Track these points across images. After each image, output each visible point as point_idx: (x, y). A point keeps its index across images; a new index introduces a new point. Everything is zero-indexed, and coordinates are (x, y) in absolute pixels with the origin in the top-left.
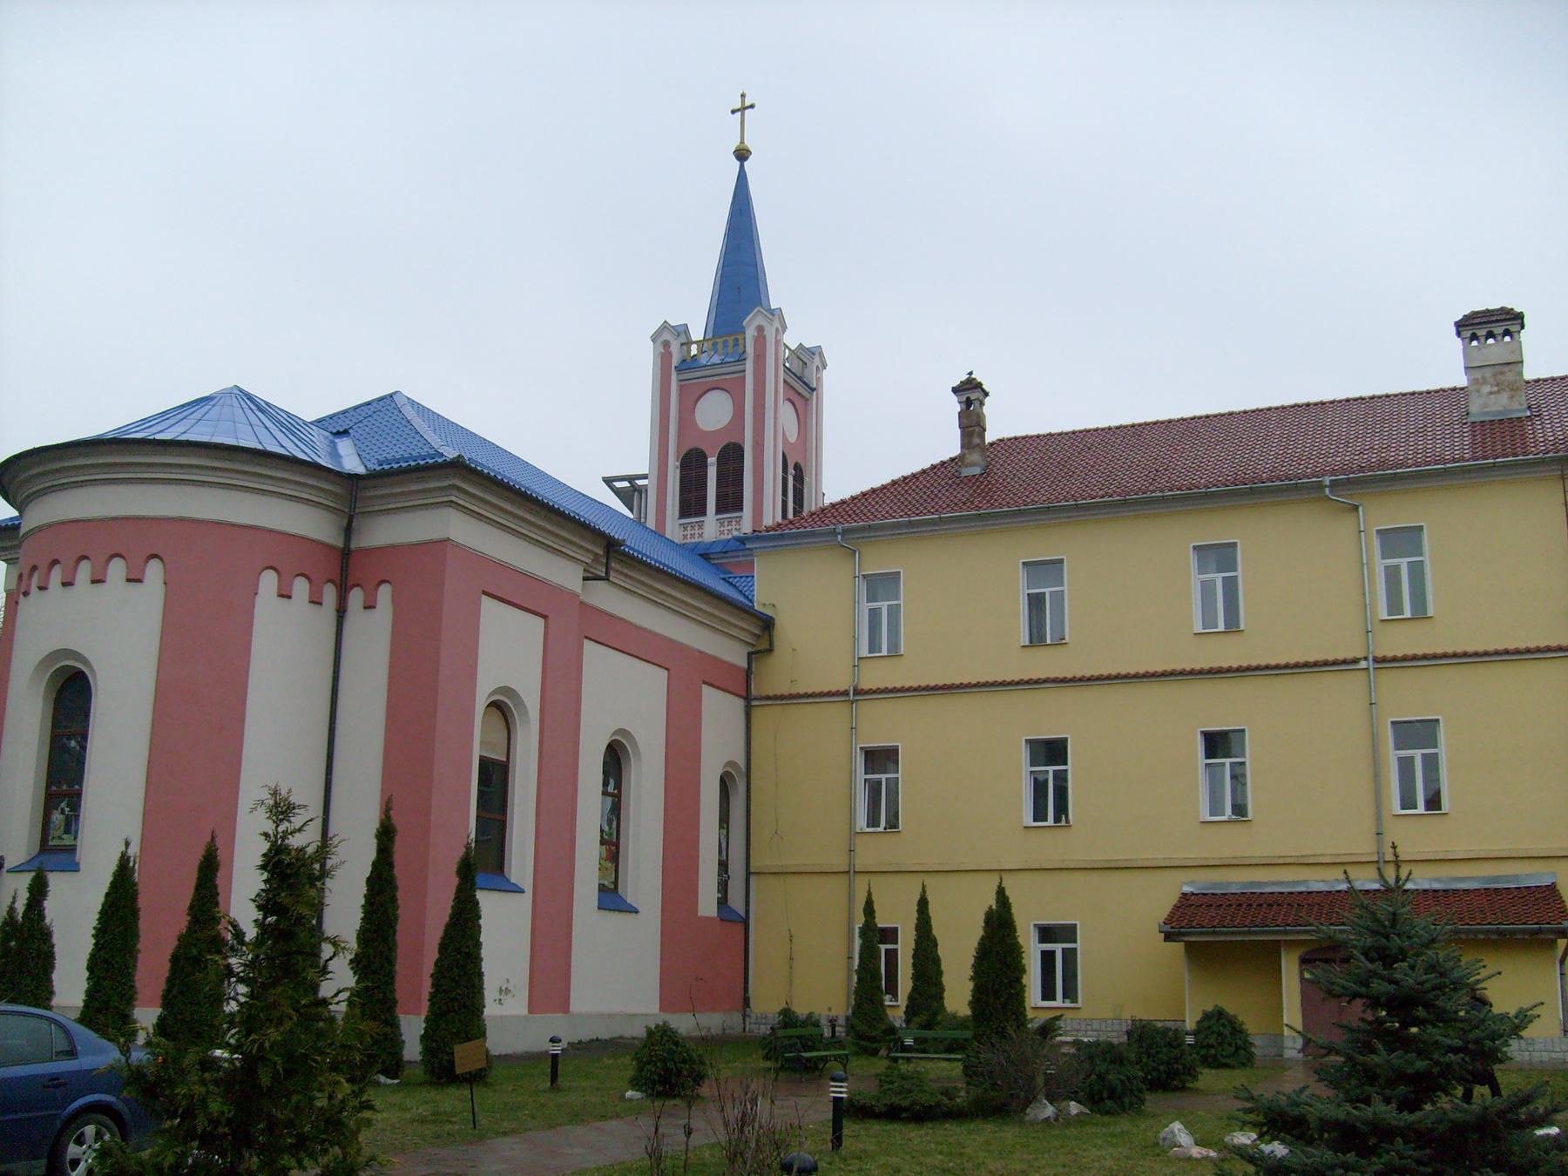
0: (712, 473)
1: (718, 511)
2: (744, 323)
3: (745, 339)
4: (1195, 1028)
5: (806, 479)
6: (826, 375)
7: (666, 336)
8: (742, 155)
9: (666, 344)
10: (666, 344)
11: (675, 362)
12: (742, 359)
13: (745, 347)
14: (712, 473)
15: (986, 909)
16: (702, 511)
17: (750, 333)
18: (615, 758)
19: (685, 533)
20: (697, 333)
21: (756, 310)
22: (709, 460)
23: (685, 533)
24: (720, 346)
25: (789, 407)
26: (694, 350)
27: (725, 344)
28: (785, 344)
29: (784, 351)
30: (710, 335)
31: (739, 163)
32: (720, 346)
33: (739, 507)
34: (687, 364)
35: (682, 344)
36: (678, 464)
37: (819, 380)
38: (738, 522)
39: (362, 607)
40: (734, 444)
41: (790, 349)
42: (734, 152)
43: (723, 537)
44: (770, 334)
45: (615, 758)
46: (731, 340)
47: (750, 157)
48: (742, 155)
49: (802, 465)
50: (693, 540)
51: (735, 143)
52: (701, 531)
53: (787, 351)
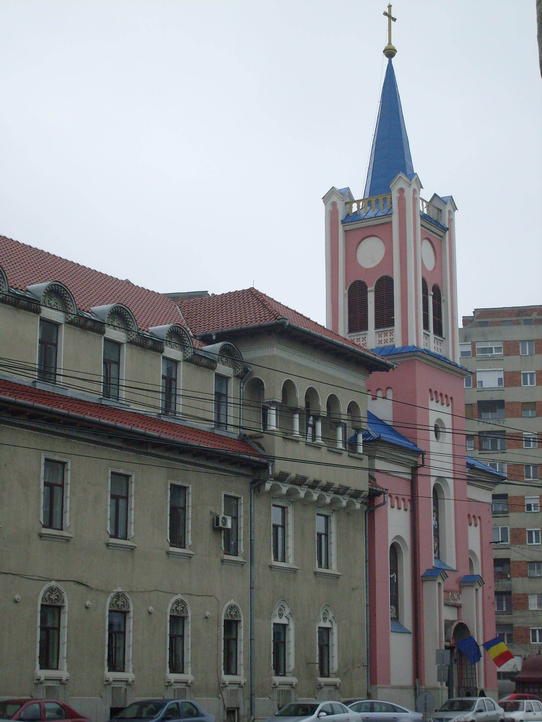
0: (371, 298)
1: (377, 326)
2: (390, 187)
3: (391, 198)
4: (367, 507)
5: (443, 298)
6: (458, 216)
7: (334, 199)
8: (390, 53)
9: (334, 204)
10: (334, 204)
11: (341, 217)
12: (389, 215)
13: (391, 203)
14: (371, 298)
15: (307, 476)
16: (365, 327)
17: (395, 195)
18: (395, 549)
19: (380, 339)
20: (358, 193)
21: (398, 177)
22: (369, 289)
23: (380, 339)
24: (373, 203)
25: (426, 243)
26: (355, 208)
27: (377, 201)
28: (421, 198)
29: (422, 204)
30: (367, 196)
31: (388, 59)
32: (373, 203)
33: (391, 323)
34: (350, 218)
35: (346, 203)
36: (346, 292)
37: (451, 220)
38: (391, 334)
39: (462, 608)
40: (386, 277)
41: (426, 201)
42: (384, 51)
43: (381, 345)
44: (408, 195)
45: (395, 549)
46: (381, 199)
47: (396, 54)
48: (390, 53)
49: (440, 286)
50: (386, 344)
51: (384, 44)
52: (391, 337)
53: (424, 203)
